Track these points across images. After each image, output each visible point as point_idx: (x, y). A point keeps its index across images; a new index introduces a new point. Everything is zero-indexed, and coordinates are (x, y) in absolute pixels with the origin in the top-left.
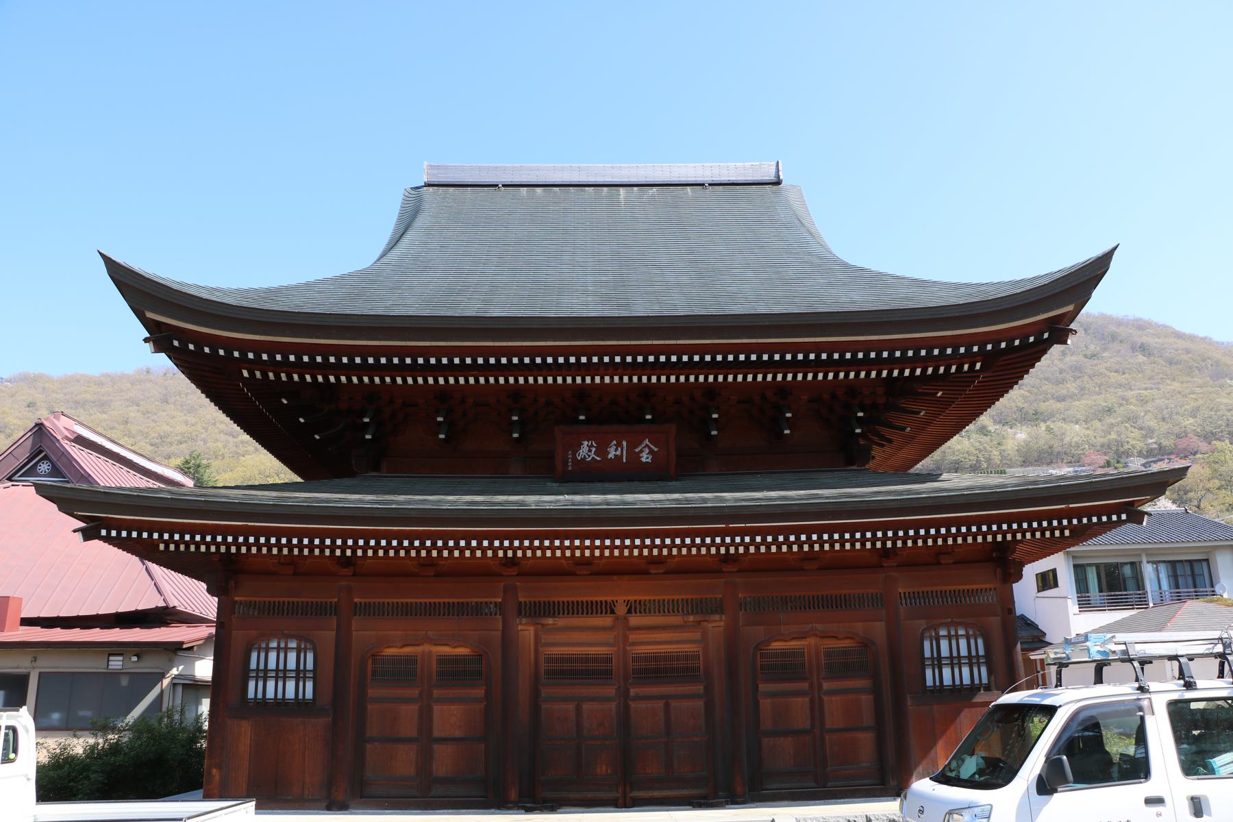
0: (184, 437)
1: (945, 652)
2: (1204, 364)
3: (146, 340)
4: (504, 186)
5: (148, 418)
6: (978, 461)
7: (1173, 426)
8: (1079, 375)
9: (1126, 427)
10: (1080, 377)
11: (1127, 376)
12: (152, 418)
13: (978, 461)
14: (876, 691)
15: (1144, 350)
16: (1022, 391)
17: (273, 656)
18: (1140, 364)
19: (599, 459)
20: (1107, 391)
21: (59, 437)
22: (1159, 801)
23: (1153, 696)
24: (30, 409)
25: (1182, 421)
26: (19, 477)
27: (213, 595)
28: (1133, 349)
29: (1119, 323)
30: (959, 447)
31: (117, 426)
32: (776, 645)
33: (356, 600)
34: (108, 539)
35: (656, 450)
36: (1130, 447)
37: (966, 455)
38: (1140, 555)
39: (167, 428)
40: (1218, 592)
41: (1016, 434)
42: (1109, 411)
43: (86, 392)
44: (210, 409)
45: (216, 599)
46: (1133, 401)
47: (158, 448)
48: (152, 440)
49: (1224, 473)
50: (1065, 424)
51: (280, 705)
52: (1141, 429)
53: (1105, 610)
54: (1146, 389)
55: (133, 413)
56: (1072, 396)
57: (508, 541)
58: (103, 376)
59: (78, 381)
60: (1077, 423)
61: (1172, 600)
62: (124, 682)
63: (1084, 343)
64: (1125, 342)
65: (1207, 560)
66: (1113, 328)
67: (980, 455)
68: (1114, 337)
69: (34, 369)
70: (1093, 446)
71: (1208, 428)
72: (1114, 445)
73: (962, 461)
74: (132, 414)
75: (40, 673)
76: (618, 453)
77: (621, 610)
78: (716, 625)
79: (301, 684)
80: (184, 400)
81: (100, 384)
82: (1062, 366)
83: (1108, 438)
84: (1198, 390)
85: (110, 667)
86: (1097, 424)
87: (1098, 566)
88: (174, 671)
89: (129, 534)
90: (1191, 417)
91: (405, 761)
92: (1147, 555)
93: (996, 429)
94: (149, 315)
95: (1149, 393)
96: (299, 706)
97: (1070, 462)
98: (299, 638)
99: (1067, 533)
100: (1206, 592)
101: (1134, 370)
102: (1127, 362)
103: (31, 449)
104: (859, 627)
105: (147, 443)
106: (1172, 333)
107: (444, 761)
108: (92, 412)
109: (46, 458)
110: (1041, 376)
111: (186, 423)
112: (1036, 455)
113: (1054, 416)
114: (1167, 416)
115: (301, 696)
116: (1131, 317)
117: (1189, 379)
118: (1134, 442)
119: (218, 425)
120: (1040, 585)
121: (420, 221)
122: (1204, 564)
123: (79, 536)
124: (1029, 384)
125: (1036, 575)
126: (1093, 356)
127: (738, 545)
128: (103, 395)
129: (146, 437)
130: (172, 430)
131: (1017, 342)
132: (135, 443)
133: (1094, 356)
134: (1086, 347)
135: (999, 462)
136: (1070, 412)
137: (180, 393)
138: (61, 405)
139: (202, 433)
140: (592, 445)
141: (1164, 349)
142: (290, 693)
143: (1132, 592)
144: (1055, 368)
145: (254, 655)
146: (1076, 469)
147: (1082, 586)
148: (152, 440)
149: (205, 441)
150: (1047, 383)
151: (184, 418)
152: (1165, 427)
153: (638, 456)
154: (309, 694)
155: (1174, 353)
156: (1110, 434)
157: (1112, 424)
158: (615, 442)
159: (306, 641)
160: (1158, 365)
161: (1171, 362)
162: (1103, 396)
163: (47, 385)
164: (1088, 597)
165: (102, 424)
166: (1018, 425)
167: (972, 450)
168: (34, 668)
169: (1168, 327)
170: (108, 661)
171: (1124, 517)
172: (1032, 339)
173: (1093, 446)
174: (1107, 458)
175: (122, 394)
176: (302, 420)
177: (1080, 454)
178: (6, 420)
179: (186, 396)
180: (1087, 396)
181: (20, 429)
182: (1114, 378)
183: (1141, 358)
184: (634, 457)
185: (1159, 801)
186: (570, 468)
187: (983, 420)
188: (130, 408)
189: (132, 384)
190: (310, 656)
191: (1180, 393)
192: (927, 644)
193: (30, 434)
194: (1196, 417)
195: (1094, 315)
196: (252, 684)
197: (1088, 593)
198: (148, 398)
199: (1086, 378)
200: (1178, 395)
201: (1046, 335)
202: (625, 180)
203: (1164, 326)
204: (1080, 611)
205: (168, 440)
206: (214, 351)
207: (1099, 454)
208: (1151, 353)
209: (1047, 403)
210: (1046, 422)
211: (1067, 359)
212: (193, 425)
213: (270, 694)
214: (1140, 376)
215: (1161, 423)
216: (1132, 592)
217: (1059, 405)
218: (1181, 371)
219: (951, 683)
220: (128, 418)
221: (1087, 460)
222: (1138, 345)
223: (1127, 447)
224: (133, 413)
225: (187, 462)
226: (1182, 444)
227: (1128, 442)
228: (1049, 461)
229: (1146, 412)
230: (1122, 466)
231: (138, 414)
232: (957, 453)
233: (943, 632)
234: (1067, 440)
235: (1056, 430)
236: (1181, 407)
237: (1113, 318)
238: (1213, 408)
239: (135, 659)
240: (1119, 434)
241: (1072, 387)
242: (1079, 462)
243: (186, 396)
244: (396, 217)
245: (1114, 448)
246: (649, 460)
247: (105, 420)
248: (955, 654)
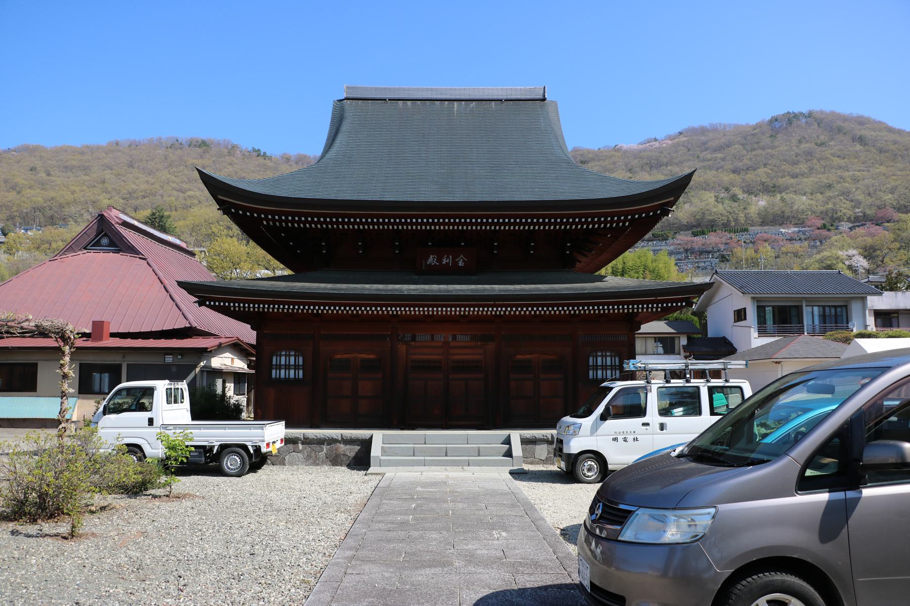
0: (146, 193)
1: (599, 363)
2: (906, 153)
3: (218, 209)
4: (389, 100)
5: (120, 178)
7: (876, 200)
8: (810, 158)
9: (841, 200)
10: (811, 160)
11: (846, 160)
12: (122, 179)
13: (729, 221)
15: (861, 140)
16: (766, 169)
17: (283, 358)
18: (857, 151)
19: (438, 264)
20: (829, 171)
21: (113, 223)
22: (647, 424)
23: (652, 385)
24: (33, 172)
25: (883, 197)
26: (91, 247)
27: (254, 330)
28: (853, 140)
29: (845, 119)
31: (96, 184)
32: (519, 357)
33: (322, 332)
34: (209, 306)
35: (466, 260)
36: (842, 214)
37: (720, 216)
38: (801, 301)
39: (134, 186)
40: (850, 327)
41: (758, 201)
42: (830, 186)
43: (72, 159)
44: (165, 172)
45: (255, 332)
46: (848, 179)
47: (128, 201)
48: (123, 195)
49: (904, 238)
50: (795, 195)
51: (287, 381)
52: (852, 201)
53: (775, 336)
54: (859, 171)
55: (108, 174)
56: (803, 175)
58: (83, 147)
59: (66, 151)
60: (805, 195)
61: (820, 331)
62: (174, 369)
63: (816, 134)
64: (848, 134)
65: (846, 306)
66: (839, 123)
67: (729, 216)
68: (840, 130)
69: (32, 141)
70: (815, 213)
71: (902, 202)
72: (831, 213)
73: (716, 220)
74: (108, 176)
75: (128, 364)
76: (448, 261)
79: (297, 371)
80: (145, 165)
81: (82, 153)
82: (798, 151)
83: (826, 207)
84: (899, 173)
85: (166, 361)
86: (819, 196)
87: (773, 307)
88: (202, 364)
89: (219, 304)
90: (890, 193)
92: (807, 301)
93: (744, 197)
94: (220, 197)
95: (861, 174)
96: (296, 380)
97: (797, 224)
98: (295, 350)
99: (659, 310)
100: (843, 326)
101: (852, 156)
102: (847, 150)
103: (97, 230)
105: (120, 198)
106: (886, 128)
108: (78, 175)
109: (105, 235)
110: (781, 158)
111: (147, 182)
112: (771, 217)
113: (788, 188)
114: (872, 192)
115: (297, 377)
116: (855, 114)
117: (893, 164)
118: (845, 211)
119: (171, 183)
120: (736, 318)
121: (345, 127)
122: (844, 309)
123: (197, 305)
124: (772, 164)
125: (734, 311)
126: (822, 144)
127: (501, 311)
128: (85, 162)
129: (118, 193)
130: (137, 187)
131: (644, 215)
132: (111, 198)
133: (823, 144)
134: (818, 137)
135: (743, 222)
136: (800, 187)
137: (141, 161)
138: (55, 170)
139: (160, 190)
140: (434, 258)
141: (877, 140)
142: (292, 376)
143: (794, 325)
144: (792, 153)
145: (274, 358)
146: (801, 229)
147: (761, 320)
148: (123, 195)
149: (162, 196)
150: (785, 164)
151: (146, 178)
152: (870, 200)
153: (457, 263)
154: (301, 376)
155: (884, 144)
156: (828, 204)
157: (830, 197)
158: (446, 256)
159: (299, 352)
160: (871, 153)
161: (881, 151)
162: (826, 175)
163: (43, 154)
164: (766, 327)
165: (86, 184)
166: (761, 194)
167: (725, 212)
168: (124, 361)
169: (882, 123)
170: (165, 358)
171: (684, 304)
172: (651, 214)
173: (815, 213)
174: (823, 222)
175: (99, 161)
176: (291, 244)
177: (805, 218)
178: (16, 180)
179: (147, 163)
180: (814, 175)
181: (26, 187)
182: (837, 161)
183: (858, 147)
184: (455, 263)
185: (647, 424)
186: (424, 268)
187: (735, 190)
188: (106, 172)
189: (106, 154)
190: (301, 359)
191: (884, 175)
192: (591, 359)
193: (96, 221)
194: (894, 193)
195: (827, 113)
196: (274, 372)
197: (765, 324)
198: (118, 164)
199: (815, 161)
200: (883, 177)
201: (659, 212)
202: (458, 97)
203: (880, 122)
204: (759, 336)
205: (135, 195)
206: (252, 214)
207: (819, 219)
208: (867, 143)
209: (784, 179)
210: (781, 194)
211: (802, 146)
212: (152, 184)
213: (283, 376)
214: (856, 160)
215: (867, 197)
216: (794, 325)
217: (792, 181)
218: (887, 158)
219: (592, 378)
220: (104, 179)
221: (809, 223)
222: (858, 137)
223: (839, 214)
224: (108, 174)
225: (154, 214)
226: (881, 213)
227: (841, 211)
228: (781, 222)
229: (857, 189)
230: (834, 228)
231: (112, 176)
232: (713, 214)
233: (599, 354)
234: (795, 207)
235: (788, 200)
236: (883, 185)
237: (841, 115)
238: (907, 187)
239: (180, 357)
240: (835, 204)
241: (803, 167)
242: (803, 224)
243: (147, 163)
244: (330, 120)
245: (830, 215)
246: (463, 265)
247: (88, 181)
248: (613, 364)
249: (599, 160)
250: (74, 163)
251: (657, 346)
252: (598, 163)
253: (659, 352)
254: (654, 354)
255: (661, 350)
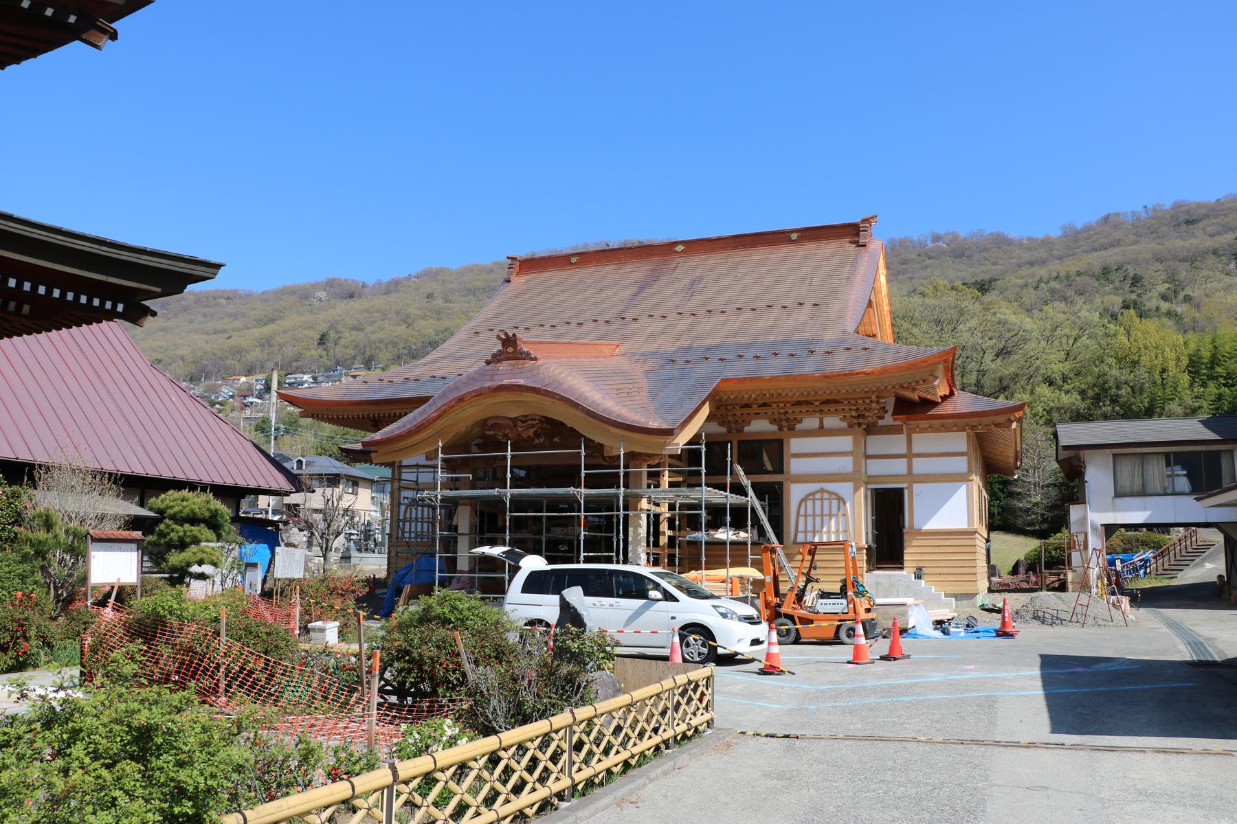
69: (435, 265)
249: (1216, 216)
250: (479, 284)
251: (1172, 476)
252: (1215, 221)
253: (1178, 489)
254: (1166, 494)
255: (1183, 483)
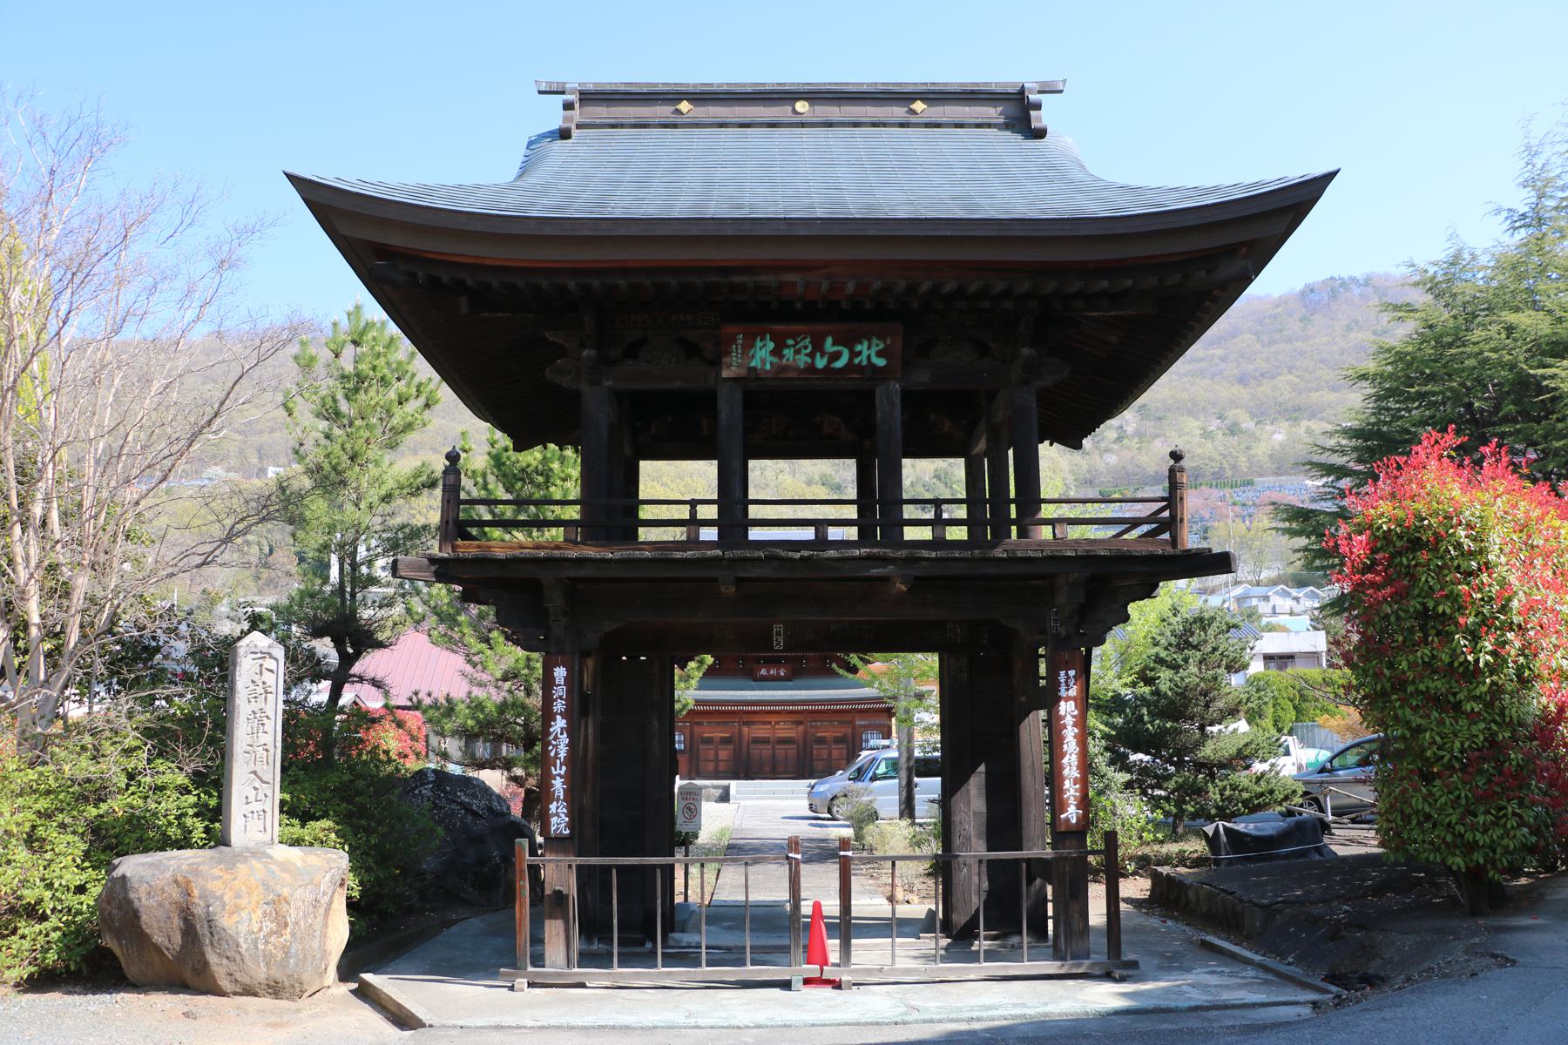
6: (1222, 468)
13: (1222, 468)
14: (848, 748)
30: (1200, 451)
37: (1207, 461)
57: (645, 466)
77: (773, 723)
78: (801, 728)
91: (711, 767)
104: (843, 730)
107: (722, 766)
133: (1385, 332)
184: (778, 674)
211: (1352, 336)
